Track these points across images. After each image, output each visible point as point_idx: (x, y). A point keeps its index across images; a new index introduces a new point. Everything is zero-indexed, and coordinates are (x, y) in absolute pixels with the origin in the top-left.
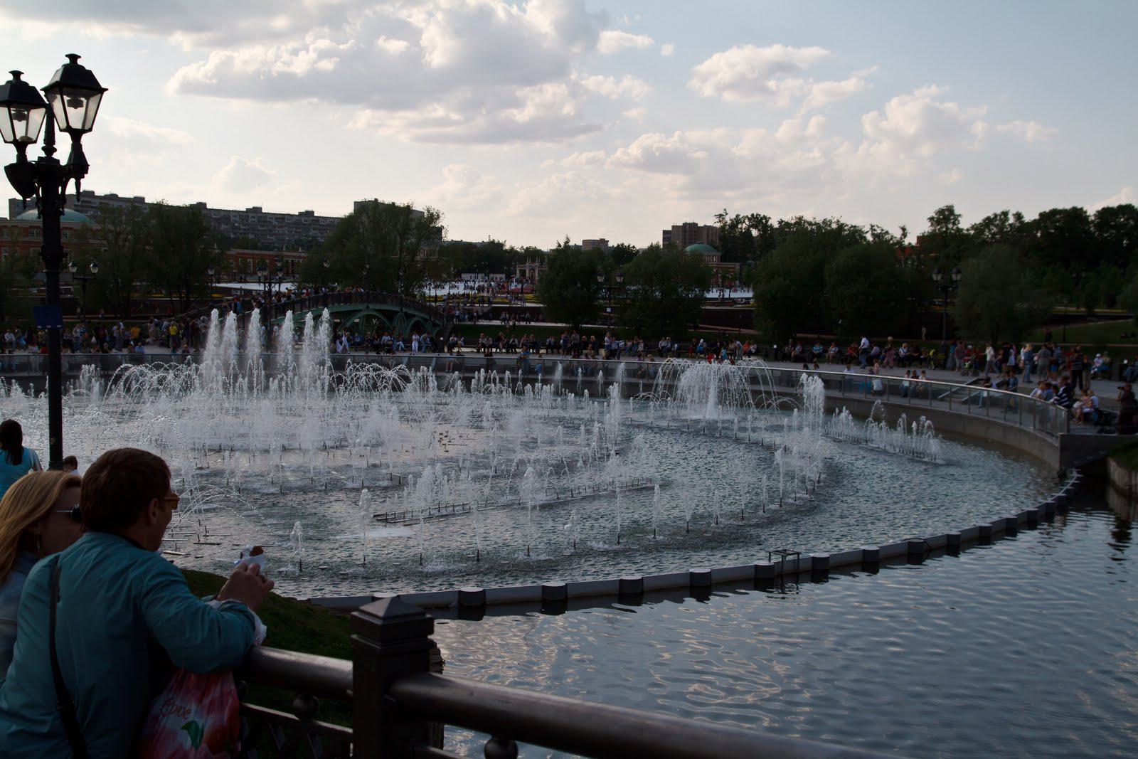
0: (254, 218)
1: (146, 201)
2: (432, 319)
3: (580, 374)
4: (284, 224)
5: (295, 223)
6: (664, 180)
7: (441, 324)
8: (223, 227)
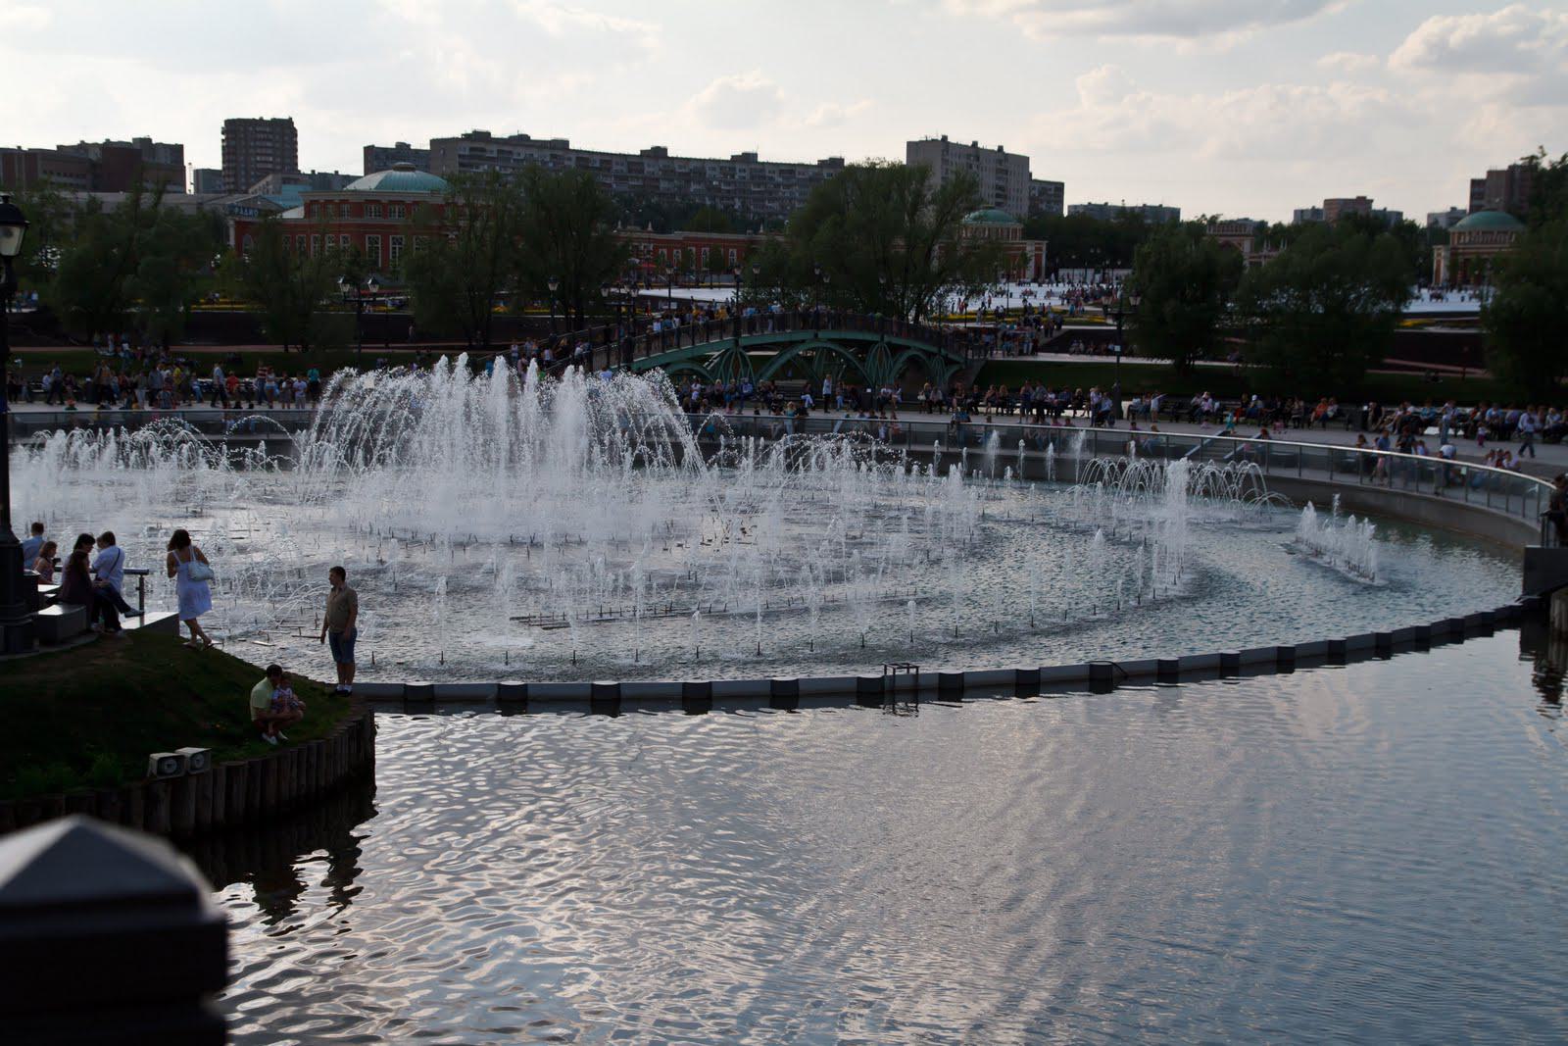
0: (744, 171)
1: (571, 147)
2: (943, 352)
3: (1021, 449)
4: (794, 181)
5: (811, 179)
6: (1473, 84)
8: (693, 187)
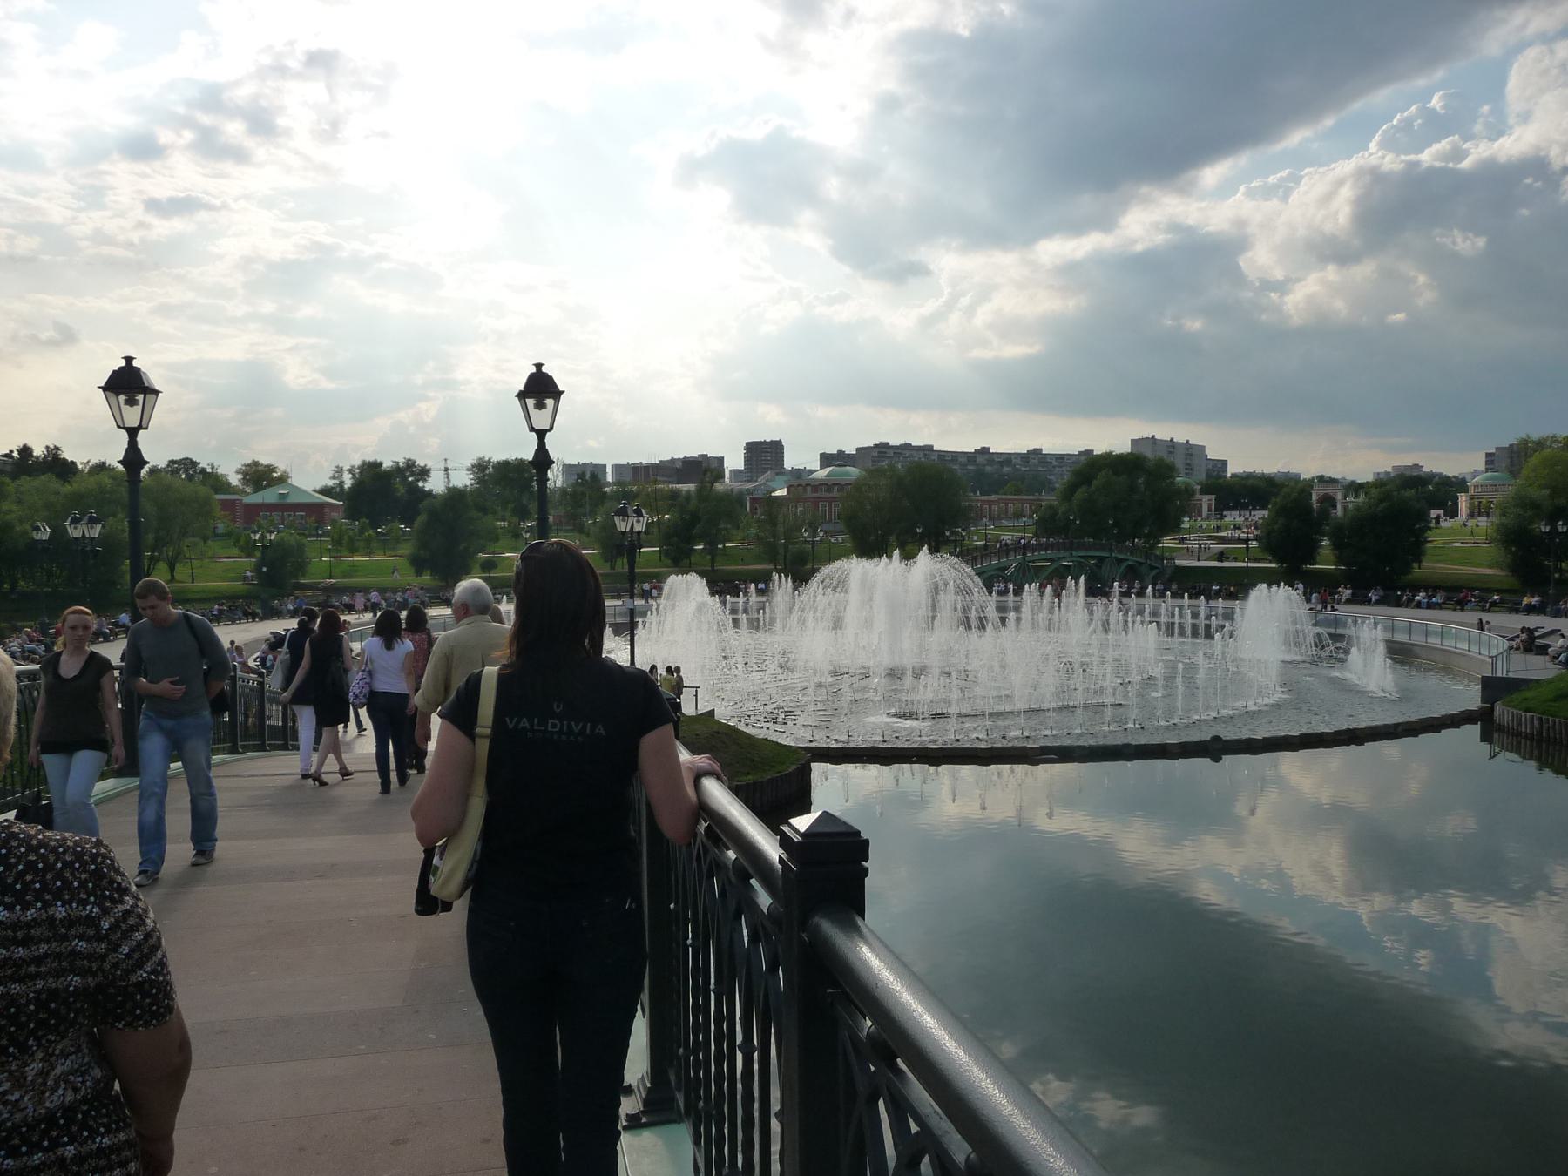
1: (935, 449)
7: (1160, 566)
